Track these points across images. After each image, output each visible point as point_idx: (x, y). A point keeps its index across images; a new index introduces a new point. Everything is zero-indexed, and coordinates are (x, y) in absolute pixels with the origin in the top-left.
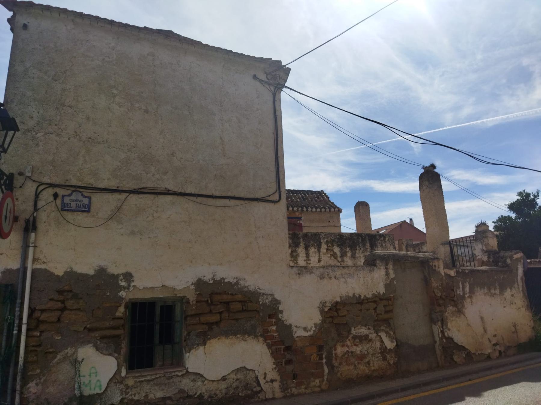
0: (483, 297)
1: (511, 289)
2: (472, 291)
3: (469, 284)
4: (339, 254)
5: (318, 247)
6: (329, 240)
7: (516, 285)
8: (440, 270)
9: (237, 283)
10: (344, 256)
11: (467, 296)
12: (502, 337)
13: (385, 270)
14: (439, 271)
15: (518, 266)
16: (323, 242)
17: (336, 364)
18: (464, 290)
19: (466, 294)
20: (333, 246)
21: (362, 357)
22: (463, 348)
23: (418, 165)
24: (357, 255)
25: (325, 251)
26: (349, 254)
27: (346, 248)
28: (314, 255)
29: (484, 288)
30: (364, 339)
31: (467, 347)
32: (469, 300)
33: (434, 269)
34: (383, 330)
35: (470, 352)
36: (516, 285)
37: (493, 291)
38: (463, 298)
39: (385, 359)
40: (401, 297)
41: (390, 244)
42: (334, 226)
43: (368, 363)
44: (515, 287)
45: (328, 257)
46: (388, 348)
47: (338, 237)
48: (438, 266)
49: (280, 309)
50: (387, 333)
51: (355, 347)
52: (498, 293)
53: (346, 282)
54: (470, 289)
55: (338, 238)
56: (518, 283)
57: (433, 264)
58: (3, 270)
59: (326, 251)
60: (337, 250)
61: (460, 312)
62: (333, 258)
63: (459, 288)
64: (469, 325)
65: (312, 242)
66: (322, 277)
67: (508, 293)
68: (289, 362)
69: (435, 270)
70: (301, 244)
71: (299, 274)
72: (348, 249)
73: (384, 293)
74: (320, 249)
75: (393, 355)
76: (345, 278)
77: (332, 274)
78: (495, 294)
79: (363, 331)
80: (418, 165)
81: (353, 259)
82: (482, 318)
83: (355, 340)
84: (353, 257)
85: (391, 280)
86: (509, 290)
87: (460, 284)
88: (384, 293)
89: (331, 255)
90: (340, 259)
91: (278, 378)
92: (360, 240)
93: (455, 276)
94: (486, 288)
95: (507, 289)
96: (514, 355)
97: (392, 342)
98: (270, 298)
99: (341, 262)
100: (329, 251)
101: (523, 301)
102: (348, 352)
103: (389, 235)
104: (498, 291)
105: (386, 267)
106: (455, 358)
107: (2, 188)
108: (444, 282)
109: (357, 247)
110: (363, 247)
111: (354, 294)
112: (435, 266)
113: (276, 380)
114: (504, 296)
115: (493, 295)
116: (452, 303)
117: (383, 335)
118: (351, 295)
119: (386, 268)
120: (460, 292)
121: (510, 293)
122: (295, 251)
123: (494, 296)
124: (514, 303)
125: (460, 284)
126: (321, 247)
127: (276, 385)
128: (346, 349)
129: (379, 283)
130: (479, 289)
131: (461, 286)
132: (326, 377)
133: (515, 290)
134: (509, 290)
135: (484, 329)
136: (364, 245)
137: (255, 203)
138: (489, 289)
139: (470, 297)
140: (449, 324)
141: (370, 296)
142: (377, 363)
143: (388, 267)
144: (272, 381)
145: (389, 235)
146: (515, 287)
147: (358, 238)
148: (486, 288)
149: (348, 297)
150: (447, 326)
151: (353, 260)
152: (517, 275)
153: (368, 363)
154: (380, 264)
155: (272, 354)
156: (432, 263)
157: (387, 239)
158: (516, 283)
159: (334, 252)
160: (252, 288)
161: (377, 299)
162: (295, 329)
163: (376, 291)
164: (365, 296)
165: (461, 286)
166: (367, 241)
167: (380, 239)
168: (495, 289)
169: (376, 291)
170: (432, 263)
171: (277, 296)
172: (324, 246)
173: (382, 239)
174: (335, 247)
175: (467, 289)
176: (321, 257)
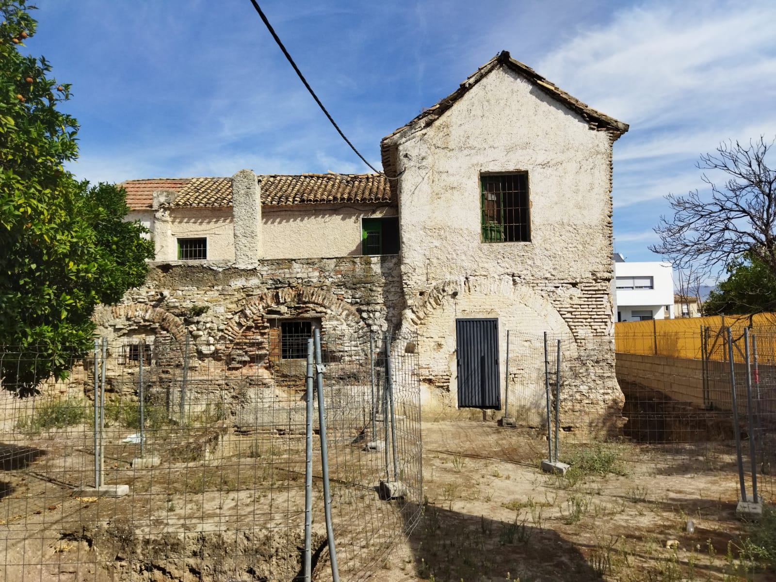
96: (307, 361)
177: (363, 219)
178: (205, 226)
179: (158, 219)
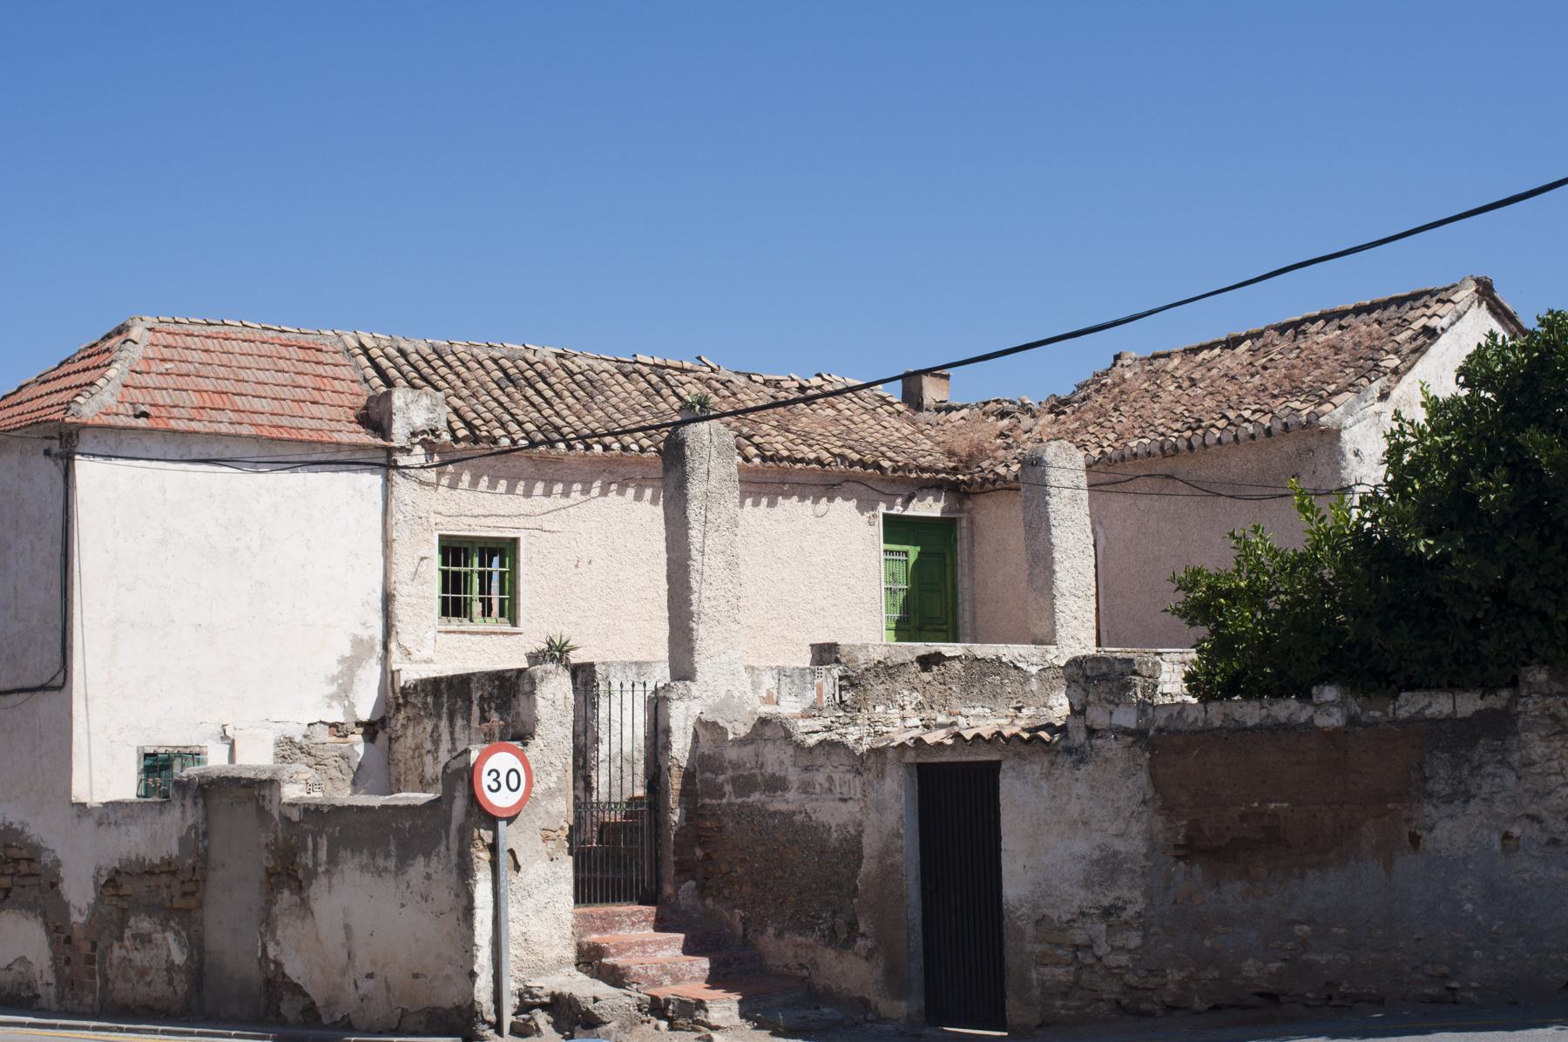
0: (358, 873)
1: (427, 855)
2: (333, 860)
7: (442, 848)
9: (22, 832)
11: (321, 869)
12: (386, 982)
16: (476, 696)
17: (111, 977)
19: (320, 865)
21: (143, 972)
22: (297, 989)
29: (361, 852)
30: (144, 939)
31: (308, 989)
32: (323, 880)
34: (172, 928)
35: (313, 1003)
36: (442, 848)
37: (380, 862)
38: (312, 874)
39: (170, 982)
40: (223, 865)
43: (149, 984)
44: (438, 855)
46: (176, 963)
49: (62, 875)
50: (177, 933)
51: (135, 952)
52: (393, 869)
53: (127, 833)
54: (329, 853)
56: (448, 843)
61: (305, 907)
63: (306, 850)
64: (318, 940)
66: (100, 824)
67: (418, 868)
68: (68, 961)
69: (263, 807)
71: (79, 816)
75: (184, 979)
76: (1522, 782)
77: (112, 818)
78: (386, 869)
79: (144, 924)
82: (347, 928)
83: (136, 939)
86: (421, 860)
87: (310, 839)
91: (54, 983)
93: (300, 821)
94: (365, 851)
95: (415, 857)
97: (183, 953)
98: (52, 855)
101: (457, 896)
102: (125, 957)
104: (392, 863)
106: (285, 1008)
111: (137, 856)
112: (264, 797)
113: (51, 984)
114: (407, 877)
115: (380, 872)
116: (294, 885)
117: (170, 936)
118: (134, 858)
120: (307, 859)
121: (422, 868)
123: (383, 874)
124: (430, 898)
125: (310, 839)
127: (52, 990)
128: (124, 953)
130: (349, 854)
131: (310, 845)
132: (98, 994)
133: (438, 862)
134: (421, 860)
135: (349, 956)
137: (39, 694)
138: (373, 856)
139: (327, 872)
140: (279, 933)
141: (157, 861)
142: (159, 988)
144: (48, 984)
146: (438, 855)
148: (365, 851)
149: (129, 860)
150: (273, 933)
152: (448, 822)
153: (149, 984)
155: (51, 944)
158: (444, 842)
160: (35, 839)
161: (168, 868)
162: (72, 909)
164: (150, 860)
165: (310, 845)
171: (59, 855)
172: (476, 711)
175: (323, 855)
176: (793, 759)
177: (885, 516)
178: (517, 503)
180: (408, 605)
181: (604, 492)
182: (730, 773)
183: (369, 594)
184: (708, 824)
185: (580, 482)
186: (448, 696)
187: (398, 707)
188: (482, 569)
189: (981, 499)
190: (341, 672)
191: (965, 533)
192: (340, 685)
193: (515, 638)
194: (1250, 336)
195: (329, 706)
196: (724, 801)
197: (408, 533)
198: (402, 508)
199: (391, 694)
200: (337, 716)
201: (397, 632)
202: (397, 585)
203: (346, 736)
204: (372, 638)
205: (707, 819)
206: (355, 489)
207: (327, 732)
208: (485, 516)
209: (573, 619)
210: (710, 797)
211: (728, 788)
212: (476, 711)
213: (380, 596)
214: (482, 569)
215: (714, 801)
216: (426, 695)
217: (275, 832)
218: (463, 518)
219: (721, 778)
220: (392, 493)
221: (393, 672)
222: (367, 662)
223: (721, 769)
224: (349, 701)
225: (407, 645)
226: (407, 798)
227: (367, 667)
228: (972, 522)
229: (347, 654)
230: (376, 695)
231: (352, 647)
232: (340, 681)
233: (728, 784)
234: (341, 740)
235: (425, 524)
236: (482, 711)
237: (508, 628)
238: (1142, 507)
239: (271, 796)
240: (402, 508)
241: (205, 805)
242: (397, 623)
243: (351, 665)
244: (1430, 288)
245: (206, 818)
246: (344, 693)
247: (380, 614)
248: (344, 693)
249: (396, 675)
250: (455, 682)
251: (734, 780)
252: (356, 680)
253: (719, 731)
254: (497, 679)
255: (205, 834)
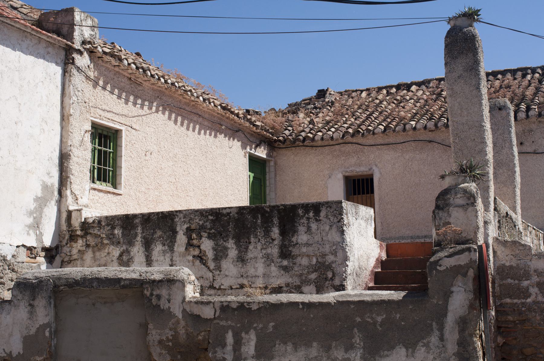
3: (257, 336)
4: (210, 254)
5: (171, 242)
6: (193, 227)
7: (434, 339)
8: (172, 307)
10: (221, 257)
13: (29, 308)
14: (169, 308)
15: (454, 289)
18: (240, 350)
20: (200, 237)
23: (439, 20)
24: (250, 255)
25: (182, 249)
26: (233, 253)
27: (228, 240)
28: (162, 258)
33: (154, 304)
41: (331, 226)
42: (535, 153)
44: (427, 345)
45: (189, 261)
47: (211, 217)
48: (167, 297)
55: (212, 220)
57: (154, 293)
58: (348, 240)
59: (186, 249)
60: (207, 245)
62: (198, 262)
63: (224, 345)
65: (159, 233)
70: (139, 238)
72: (231, 244)
73: (19, 353)
74: (174, 245)
80: (439, 20)
81: (240, 263)
84: (241, 259)
85: (38, 328)
88: (19, 353)
89: (194, 256)
90: (212, 265)
92: (259, 221)
94: (315, 344)
95: (393, 348)
99: (214, 271)
100: (191, 249)
103: (329, 204)
105: (31, 302)
107: (175, 118)
108: (182, 332)
109: (252, 236)
110: (264, 236)
119: (30, 305)
122: (128, 252)
126: (175, 242)
129: (11, 335)
136: (267, 232)
143: (36, 303)
145: (329, 204)
147: (256, 218)
151: (240, 266)
154: (19, 298)
156: (152, 290)
157: (323, 214)
158: (437, 333)
159: (200, 249)
163: (4, 349)
166: (276, 221)
167: (306, 215)
168: (349, 347)
169: (4, 349)
170: (152, 290)
172: (181, 239)
173: (311, 214)
174: (203, 239)
178: (131, 109)
179: (78, 69)
180: (77, 163)
181: (157, 111)
182: (535, 279)
183: (52, 152)
184: (510, 318)
185: (148, 101)
186: (143, 229)
187: (73, 238)
188: (100, 148)
189: (283, 151)
190: (35, 208)
191: (272, 169)
192: (35, 218)
193: (119, 197)
194: (385, 88)
195: (28, 234)
196: (529, 300)
197: (78, 111)
198: (77, 93)
199: (64, 227)
200: (31, 242)
201: (71, 182)
202: (72, 148)
203: (35, 258)
204: (52, 185)
205: (508, 314)
206: (47, 73)
207: (25, 254)
208: (108, 112)
209: (143, 189)
210: (510, 297)
211: (534, 291)
212: (181, 239)
213: (58, 155)
214: (100, 148)
215: (515, 301)
216: (113, 228)
217: (175, 329)
218: (98, 109)
219: (525, 283)
220: (70, 81)
221: (70, 213)
222: (50, 203)
223: (527, 275)
224: (39, 231)
225: (76, 193)
226: (377, 295)
227: (50, 207)
228: (276, 163)
229: (39, 195)
230: (53, 228)
231: (42, 190)
232: (35, 215)
233: (533, 287)
234: (33, 260)
235: (88, 107)
236: (190, 238)
237: (111, 189)
238: (407, 157)
239: (169, 295)
240: (77, 93)
241: (55, 306)
242: (71, 176)
243: (41, 202)
244: (524, 66)
245: (57, 316)
246: (36, 225)
247: (58, 168)
248: (36, 225)
249: (73, 215)
250: (304, 205)
251: (539, 285)
252: (43, 216)
253: (521, 248)
254: (211, 215)
255: (56, 332)
